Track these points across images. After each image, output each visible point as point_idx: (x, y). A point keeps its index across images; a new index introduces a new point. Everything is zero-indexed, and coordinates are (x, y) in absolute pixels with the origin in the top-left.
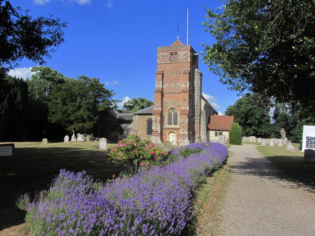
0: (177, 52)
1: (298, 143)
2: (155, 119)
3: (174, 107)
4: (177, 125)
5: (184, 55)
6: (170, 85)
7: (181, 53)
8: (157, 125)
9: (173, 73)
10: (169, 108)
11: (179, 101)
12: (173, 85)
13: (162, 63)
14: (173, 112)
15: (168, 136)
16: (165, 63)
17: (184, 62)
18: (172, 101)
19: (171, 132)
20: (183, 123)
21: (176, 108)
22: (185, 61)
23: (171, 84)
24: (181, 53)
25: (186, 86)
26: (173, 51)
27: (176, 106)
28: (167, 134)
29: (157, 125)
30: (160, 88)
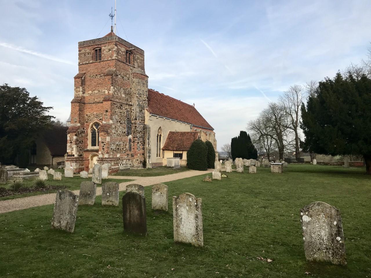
0: (100, 47)
1: (184, 122)
2: (70, 138)
3: (97, 121)
4: (95, 145)
6: (93, 92)
8: (73, 147)
9: (96, 75)
10: (91, 123)
12: (96, 92)
13: (84, 63)
14: (97, 128)
15: (90, 160)
16: (87, 62)
17: (109, 59)
19: (94, 155)
20: (103, 142)
22: (110, 59)
23: (94, 90)
25: (109, 92)
28: (90, 158)
29: (73, 147)
30: (79, 96)
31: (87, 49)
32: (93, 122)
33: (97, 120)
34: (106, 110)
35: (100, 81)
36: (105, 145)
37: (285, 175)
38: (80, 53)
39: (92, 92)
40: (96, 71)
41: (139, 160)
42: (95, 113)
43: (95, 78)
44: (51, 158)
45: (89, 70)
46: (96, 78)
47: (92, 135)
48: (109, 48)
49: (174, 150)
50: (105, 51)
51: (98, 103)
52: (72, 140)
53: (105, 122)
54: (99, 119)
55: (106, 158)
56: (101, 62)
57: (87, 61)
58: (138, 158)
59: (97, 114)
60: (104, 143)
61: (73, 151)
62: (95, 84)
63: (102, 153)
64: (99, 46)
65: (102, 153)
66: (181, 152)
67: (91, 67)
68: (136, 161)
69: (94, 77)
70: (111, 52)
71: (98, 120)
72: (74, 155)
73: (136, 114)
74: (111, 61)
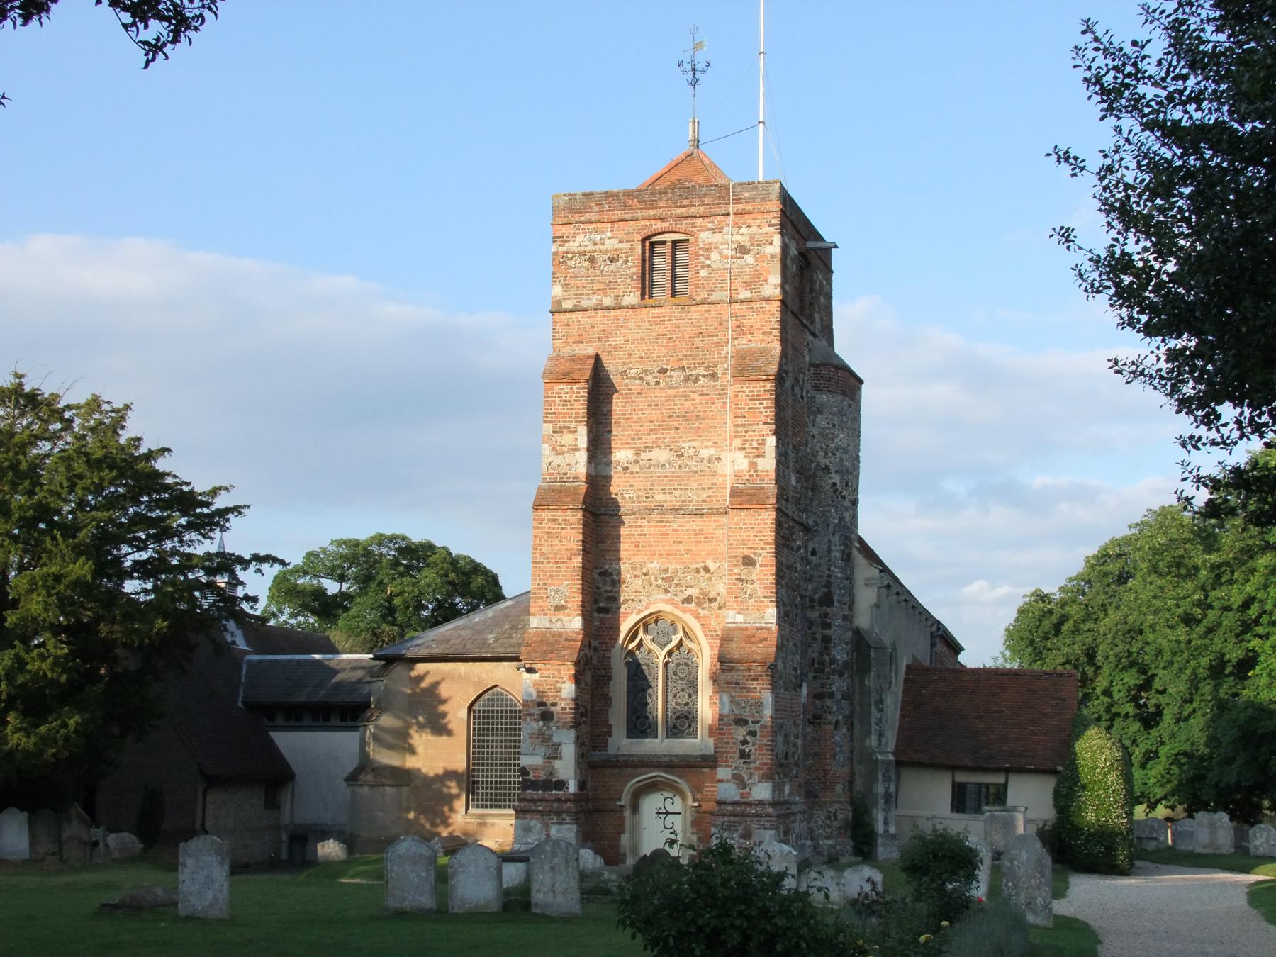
5: (742, 250)
6: (644, 456)
7: (716, 238)
8: (556, 739)
11: (706, 569)
12: (660, 455)
13: (584, 303)
15: (627, 813)
16: (608, 301)
17: (741, 296)
23: (649, 448)
25: (753, 465)
27: (688, 600)
28: (625, 800)
29: (556, 739)
31: (609, 234)
32: (640, 611)
33: (671, 602)
35: (687, 404)
38: (565, 249)
39: (637, 455)
40: (663, 351)
41: (840, 816)
42: (654, 565)
43: (658, 383)
44: (200, 795)
45: (620, 341)
46: (662, 383)
47: (630, 679)
48: (738, 238)
49: (953, 768)
50: (715, 255)
51: (675, 511)
53: (740, 618)
54: (682, 597)
55: (761, 803)
56: (693, 308)
57: (605, 295)
58: (836, 806)
60: (751, 727)
61: (557, 764)
62: (655, 415)
64: (682, 228)
66: (1000, 779)
67: (632, 326)
68: (829, 818)
69: (649, 378)
70: (749, 259)
72: (561, 785)
73: (829, 576)
74: (753, 305)
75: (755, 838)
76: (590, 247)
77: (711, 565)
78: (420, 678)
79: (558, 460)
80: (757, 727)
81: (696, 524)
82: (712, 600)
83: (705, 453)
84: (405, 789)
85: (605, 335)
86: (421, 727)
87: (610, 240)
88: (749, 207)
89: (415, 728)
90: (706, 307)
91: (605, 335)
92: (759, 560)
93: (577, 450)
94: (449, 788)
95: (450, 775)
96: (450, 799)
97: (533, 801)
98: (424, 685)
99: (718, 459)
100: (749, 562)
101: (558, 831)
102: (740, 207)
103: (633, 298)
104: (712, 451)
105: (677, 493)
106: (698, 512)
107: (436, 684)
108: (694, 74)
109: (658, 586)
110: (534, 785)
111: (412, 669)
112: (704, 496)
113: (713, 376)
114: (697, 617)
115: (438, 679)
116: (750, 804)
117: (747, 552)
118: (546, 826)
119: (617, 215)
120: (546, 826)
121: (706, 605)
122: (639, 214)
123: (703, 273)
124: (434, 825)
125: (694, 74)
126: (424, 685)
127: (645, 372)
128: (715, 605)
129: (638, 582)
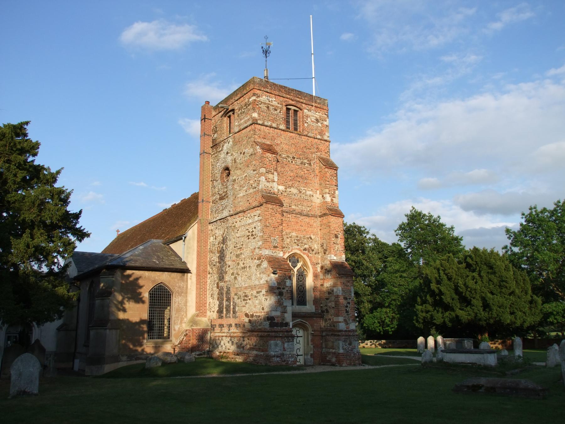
3: (298, 252)
5: (317, 121)
7: (309, 113)
8: (285, 304)
11: (311, 238)
12: (294, 191)
13: (266, 123)
16: (274, 125)
18: (294, 234)
21: (305, 256)
22: (319, 137)
23: (290, 187)
24: (309, 113)
25: (332, 200)
26: (293, 103)
27: (305, 249)
29: (285, 304)
33: (299, 250)
34: (335, 235)
36: (349, 303)
37: (234, 308)
39: (286, 189)
40: (294, 150)
42: (294, 234)
43: (292, 162)
45: (279, 142)
50: (309, 119)
52: (284, 289)
53: (335, 258)
56: (303, 137)
57: (273, 122)
59: (297, 237)
61: (286, 315)
63: (345, 320)
64: (299, 106)
65: (345, 321)
69: (289, 159)
70: (319, 124)
71: (300, 250)
72: (287, 324)
75: (353, 345)
76: (267, 102)
77: (313, 237)
78: (130, 276)
79: (268, 184)
80: (350, 301)
81: (307, 220)
82: (313, 250)
83: (309, 193)
84: (118, 331)
85: (273, 139)
86: (129, 299)
87: (274, 101)
88: (319, 106)
89: (127, 299)
90: (307, 138)
91: (273, 139)
92: (339, 236)
93: (274, 181)
94: (143, 328)
95: (142, 322)
96: (142, 333)
97: (277, 332)
98: (131, 279)
99: (313, 196)
100: (336, 237)
101: (288, 345)
102: (316, 105)
103: (283, 127)
104: (311, 193)
105: (300, 206)
106: (307, 215)
107: (137, 279)
108: (266, 52)
109: (295, 243)
110: (277, 325)
111: (124, 272)
112: (308, 209)
113: (310, 164)
114: (308, 257)
115: (138, 277)
116: (349, 331)
117: (336, 233)
118: (283, 343)
119: (277, 93)
120: (283, 343)
121: (311, 252)
122: (284, 95)
123: (306, 125)
124: (134, 346)
125: (266, 52)
126: (131, 279)
127: (288, 156)
128: (314, 252)
129: (289, 240)
